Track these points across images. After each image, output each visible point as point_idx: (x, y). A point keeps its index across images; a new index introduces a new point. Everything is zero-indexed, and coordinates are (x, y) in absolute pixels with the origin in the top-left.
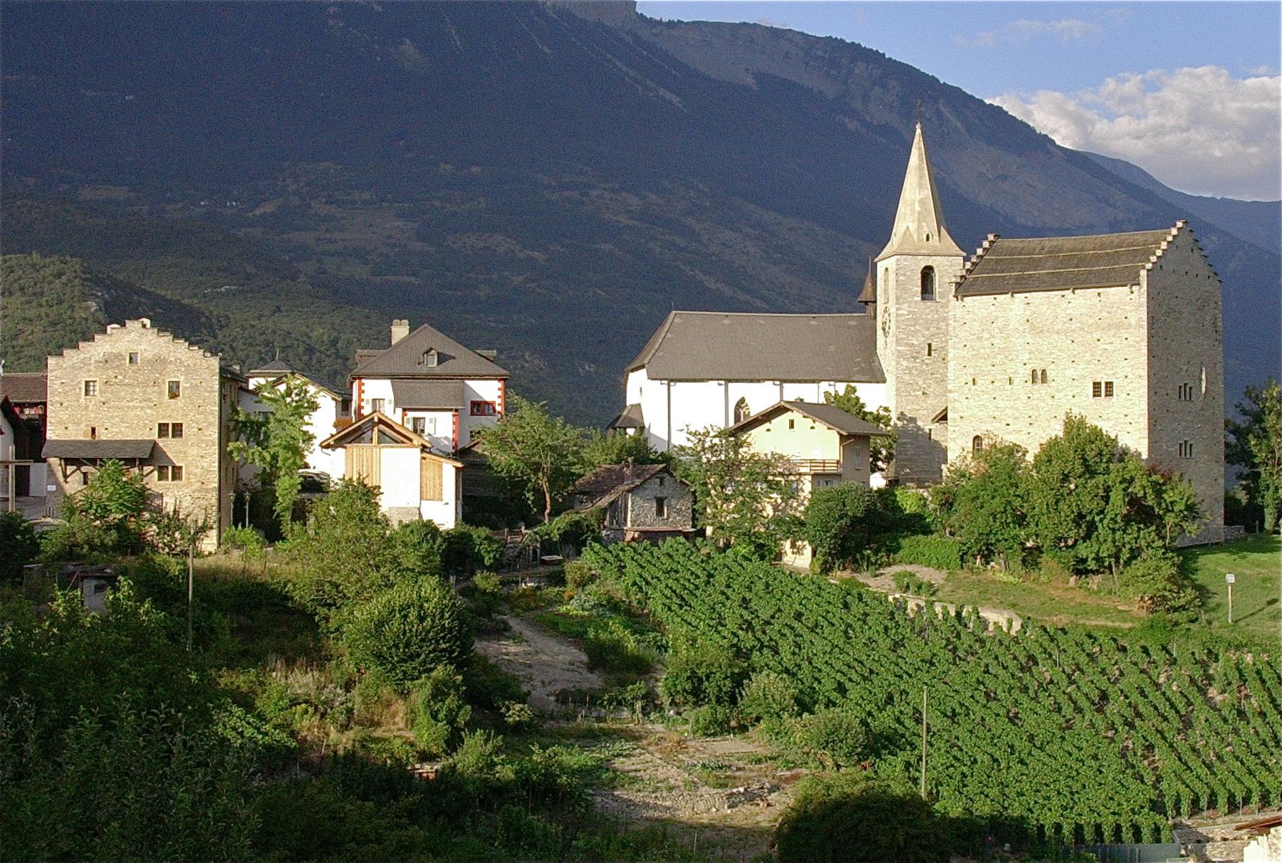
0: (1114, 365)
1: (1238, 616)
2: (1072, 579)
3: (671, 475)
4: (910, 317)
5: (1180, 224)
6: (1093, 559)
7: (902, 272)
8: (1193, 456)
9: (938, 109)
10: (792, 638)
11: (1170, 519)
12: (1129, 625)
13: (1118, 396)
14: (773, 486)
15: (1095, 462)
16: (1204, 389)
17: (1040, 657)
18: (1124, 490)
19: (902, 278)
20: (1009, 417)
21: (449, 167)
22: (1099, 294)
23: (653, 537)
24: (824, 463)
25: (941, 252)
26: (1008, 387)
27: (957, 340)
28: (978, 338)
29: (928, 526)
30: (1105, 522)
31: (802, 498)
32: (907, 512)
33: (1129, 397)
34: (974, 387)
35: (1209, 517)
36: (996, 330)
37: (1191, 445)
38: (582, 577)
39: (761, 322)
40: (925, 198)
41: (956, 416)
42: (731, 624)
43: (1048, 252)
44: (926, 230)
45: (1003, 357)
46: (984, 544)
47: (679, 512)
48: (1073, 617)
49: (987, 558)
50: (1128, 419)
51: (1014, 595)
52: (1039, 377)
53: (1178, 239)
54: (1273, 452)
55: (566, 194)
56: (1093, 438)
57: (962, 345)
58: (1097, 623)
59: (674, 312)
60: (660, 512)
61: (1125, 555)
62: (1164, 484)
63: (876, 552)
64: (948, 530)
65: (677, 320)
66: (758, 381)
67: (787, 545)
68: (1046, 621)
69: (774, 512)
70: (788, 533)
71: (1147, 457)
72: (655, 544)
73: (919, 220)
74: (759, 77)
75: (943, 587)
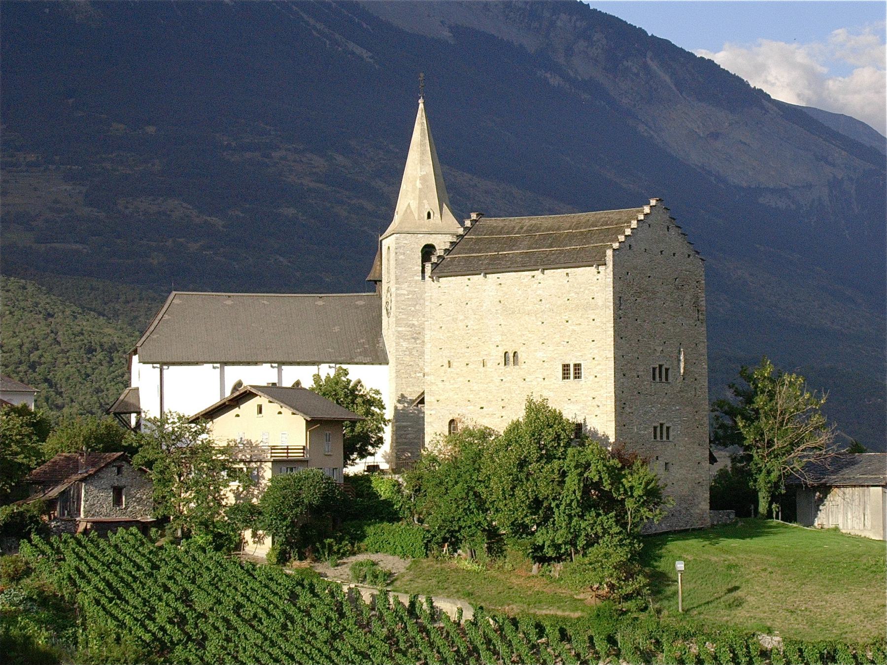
0: (582, 346)
1: (693, 604)
2: (535, 567)
3: (129, 462)
4: (410, 296)
5: (653, 202)
6: (549, 546)
7: (401, 251)
8: (671, 439)
9: (645, 63)
10: (223, 630)
11: (630, 504)
12: (578, 614)
13: (586, 378)
14: (233, 474)
15: (552, 446)
16: (682, 371)
17: (482, 648)
18: (581, 474)
19: (402, 257)
20: (484, 400)
21: (122, 126)
22: (567, 274)
23: (103, 528)
24: (288, 449)
25: (443, 231)
26: (481, 369)
27: (433, 322)
28: (453, 319)
29: (396, 512)
30: (562, 507)
31: (263, 485)
32: (382, 499)
33: (596, 379)
34: (449, 370)
35: (672, 502)
36: (470, 311)
37: (668, 428)
38: (16, 570)
39: (265, 302)
40: (427, 175)
41: (433, 399)
42: (161, 617)
43: (526, 231)
44: (427, 208)
45: (477, 338)
46: (448, 531)
47: (140, 501)
48: (525, 606)
49: (455, 546)
50: (596, 402)
51: (473, 584)
52: (511, 359)
53: (651, 217)
54: (762, 434)
55: (248, 155)
56: (551, 421)
57: (438, 326)
58: (548, 612)
59: (174, 293)
60: (117, 501)
61: (581, 542)
62: (623, 468)
63: (339, 541)
64: (416, 517)
65: (176, 301)
66: (256, 363)
67: (248, 534)
68: (498, 610)
69: (236, 500)
70: (247, 523)
71: (614, 440)
72: (104, 536)
73: (420, 198)
74: (456, 30)
75: (403, 575)
